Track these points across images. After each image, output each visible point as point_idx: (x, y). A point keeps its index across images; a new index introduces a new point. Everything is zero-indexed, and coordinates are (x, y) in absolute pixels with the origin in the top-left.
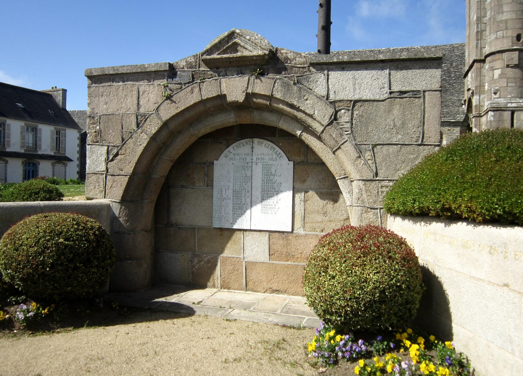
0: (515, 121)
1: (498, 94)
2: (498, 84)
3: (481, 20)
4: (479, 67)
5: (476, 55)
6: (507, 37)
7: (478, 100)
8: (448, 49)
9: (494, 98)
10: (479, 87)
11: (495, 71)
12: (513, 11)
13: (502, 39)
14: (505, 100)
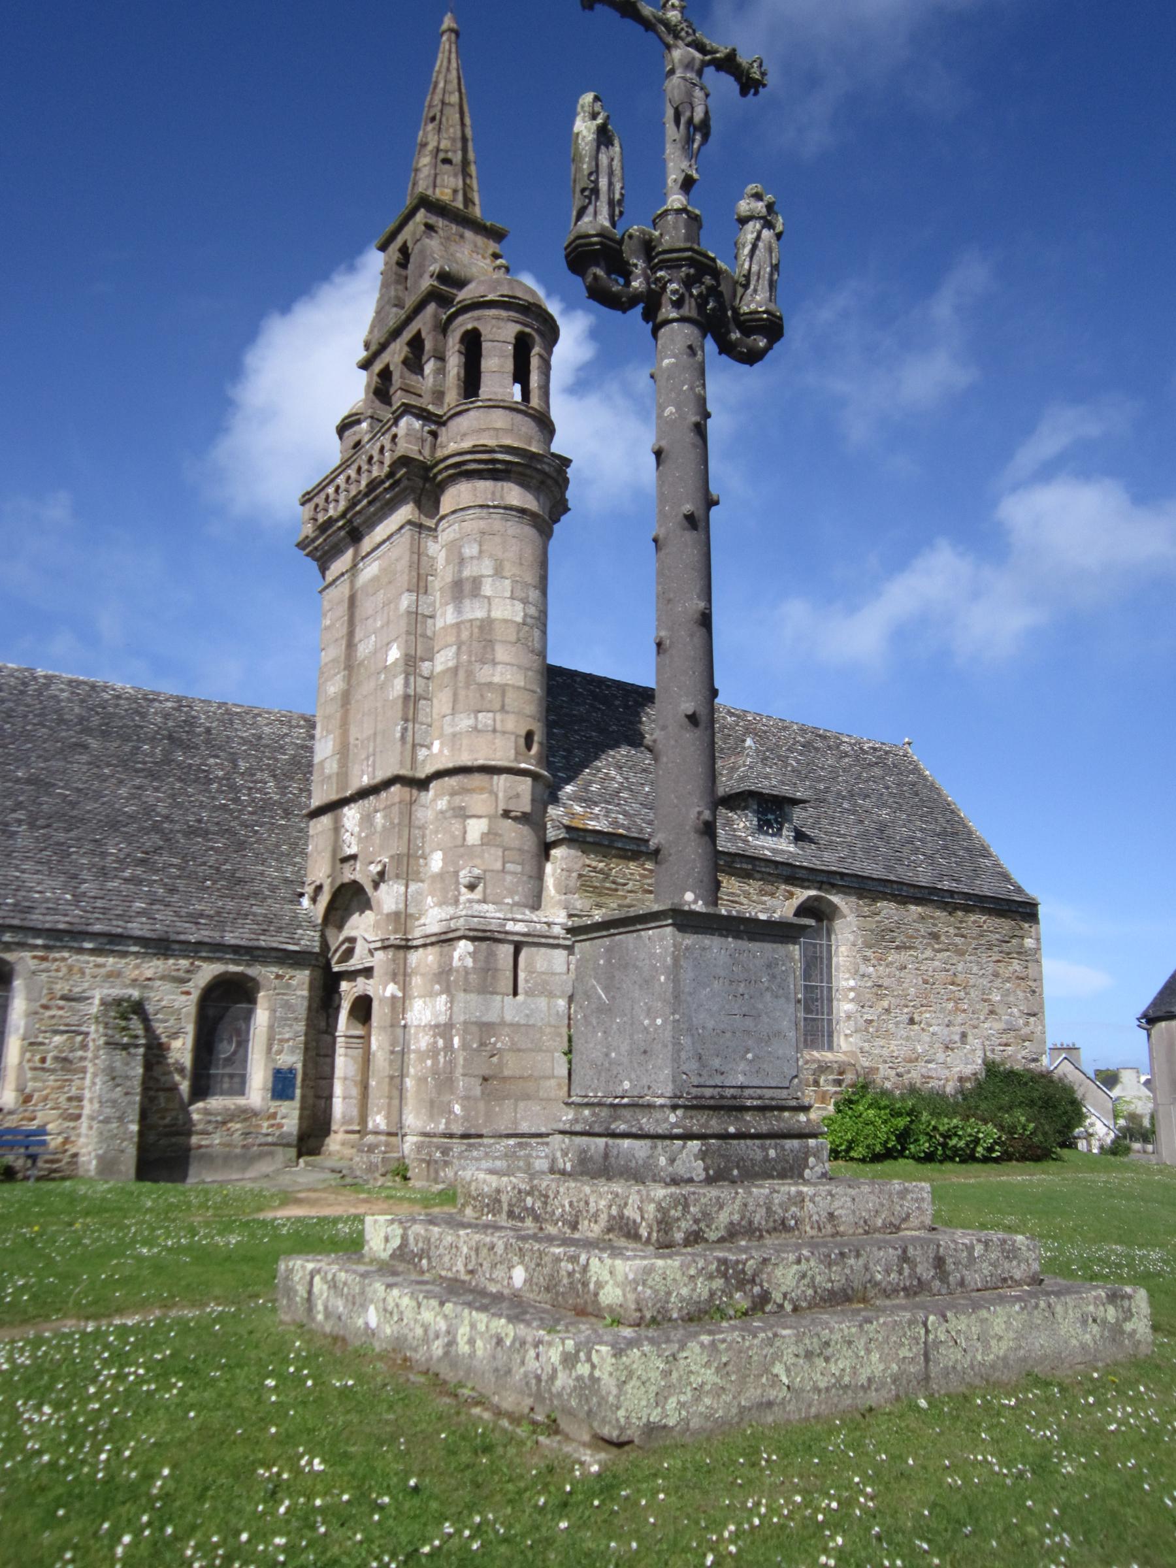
0: (522, 975)
1: (480, 888)
2: (478, 861)
3: (415, 666)
4: (408, 798)
5: (402, 763)
6: (504, 733)
7: (403, 898)
8: (215, 713)
9: (470, 901)
10: (405, 859)
11: (471, 822)
12: (519, 667)
13: (490, 736)
14: (500, 911)
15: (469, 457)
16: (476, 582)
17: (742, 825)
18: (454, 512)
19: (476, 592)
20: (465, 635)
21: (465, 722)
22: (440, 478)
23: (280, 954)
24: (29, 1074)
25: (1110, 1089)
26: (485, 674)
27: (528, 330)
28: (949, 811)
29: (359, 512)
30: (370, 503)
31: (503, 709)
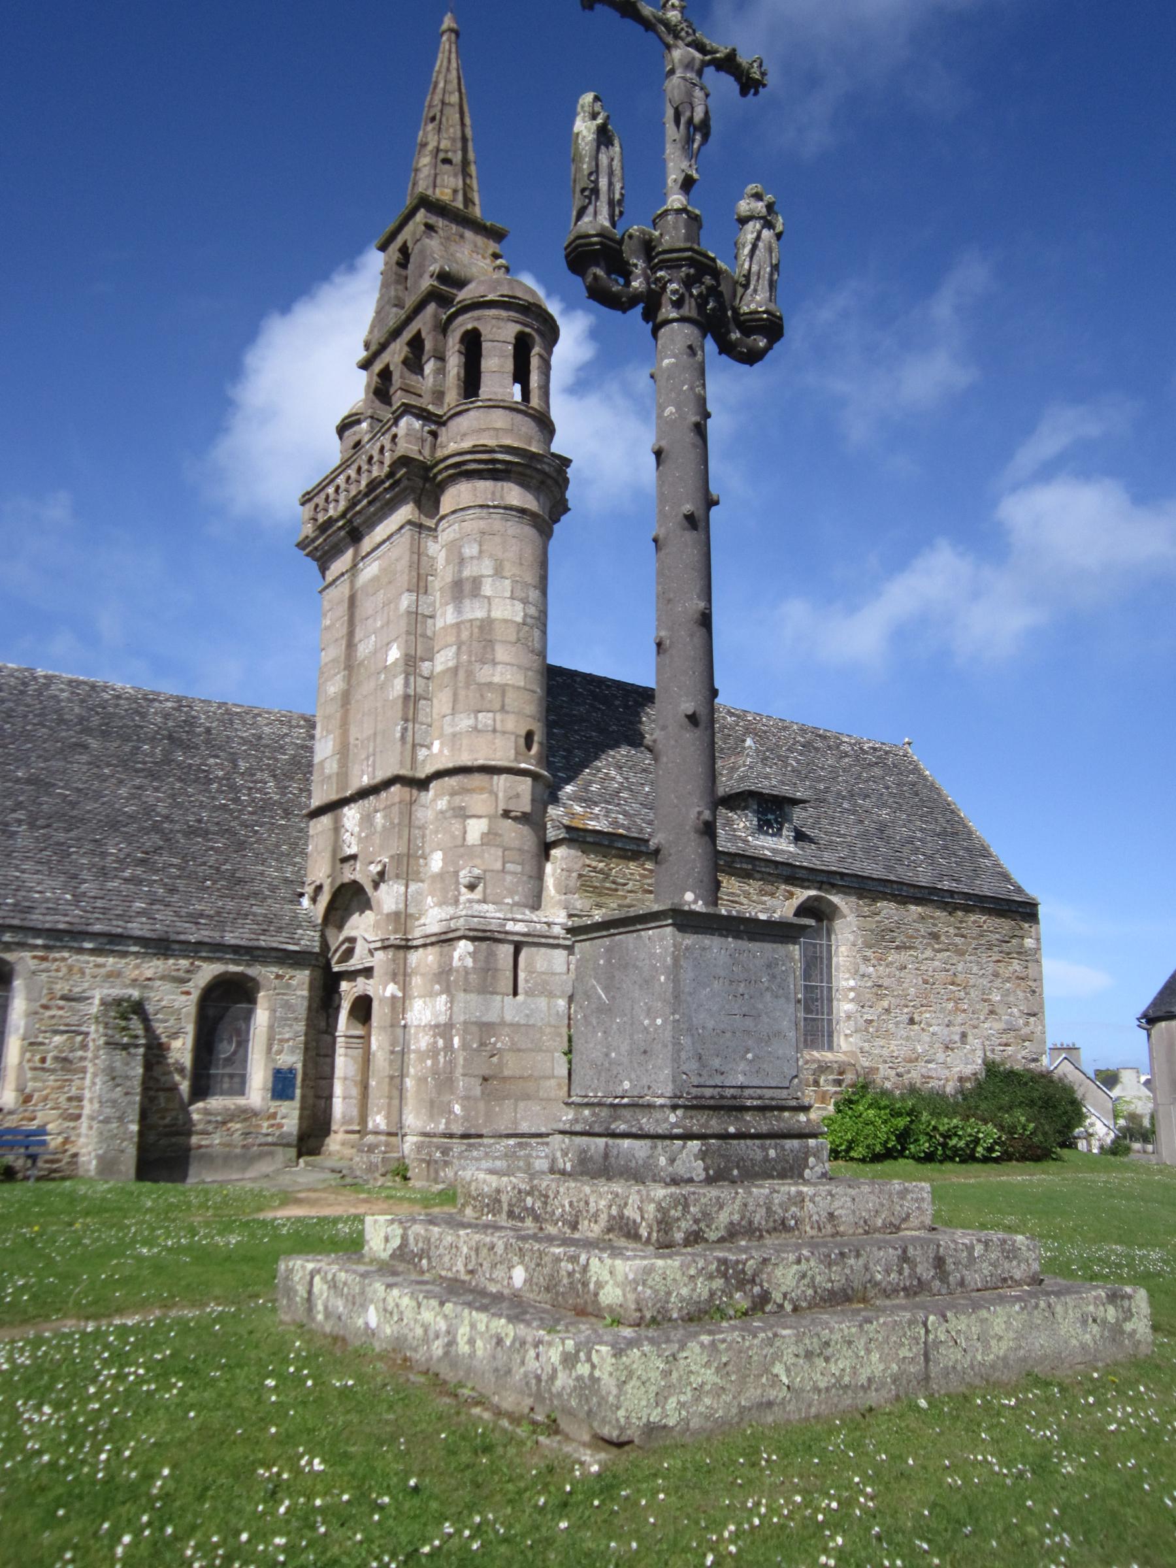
0: (522, 975)
1: (480, 888)
2: (478, 861)
3: (415, 666)
4: (408, 798)
5: (402, 763)
6: (504, 733)
7: (403, 898)
8: (215, 713)
9: (470, 901)
10: (405, 859)
11: (471, 822)
12: (519, 667)
13: (490, 736)
14: (500, 911)
15: (469, 457)
16: (476, 582)
17: (742, 825)
18: (454, 512)
19: (476, 592)
20: (465, 635)
21: (465, 722)
22: (440, 478)
23: (280, 954)
24: (29, 1074)
25: (1110, 1089)
26: (485, 674)
27: (528, 330)
28: (949, 811)
29: (359, 512)
30: (370, 503)
31: (503, 709)
